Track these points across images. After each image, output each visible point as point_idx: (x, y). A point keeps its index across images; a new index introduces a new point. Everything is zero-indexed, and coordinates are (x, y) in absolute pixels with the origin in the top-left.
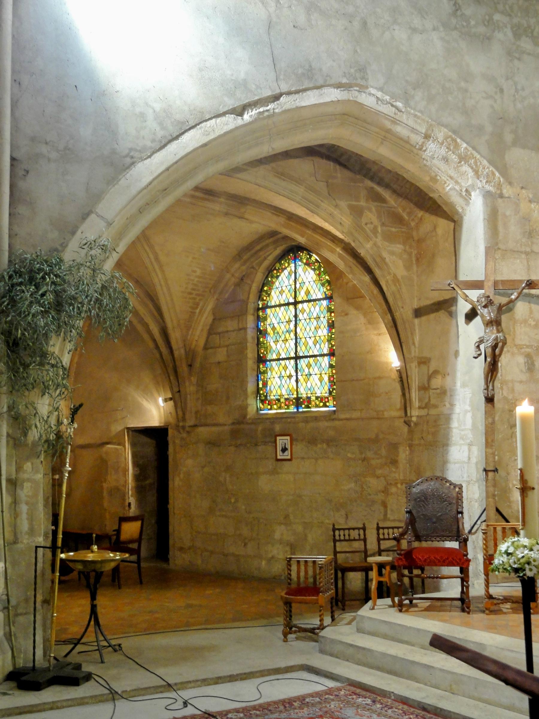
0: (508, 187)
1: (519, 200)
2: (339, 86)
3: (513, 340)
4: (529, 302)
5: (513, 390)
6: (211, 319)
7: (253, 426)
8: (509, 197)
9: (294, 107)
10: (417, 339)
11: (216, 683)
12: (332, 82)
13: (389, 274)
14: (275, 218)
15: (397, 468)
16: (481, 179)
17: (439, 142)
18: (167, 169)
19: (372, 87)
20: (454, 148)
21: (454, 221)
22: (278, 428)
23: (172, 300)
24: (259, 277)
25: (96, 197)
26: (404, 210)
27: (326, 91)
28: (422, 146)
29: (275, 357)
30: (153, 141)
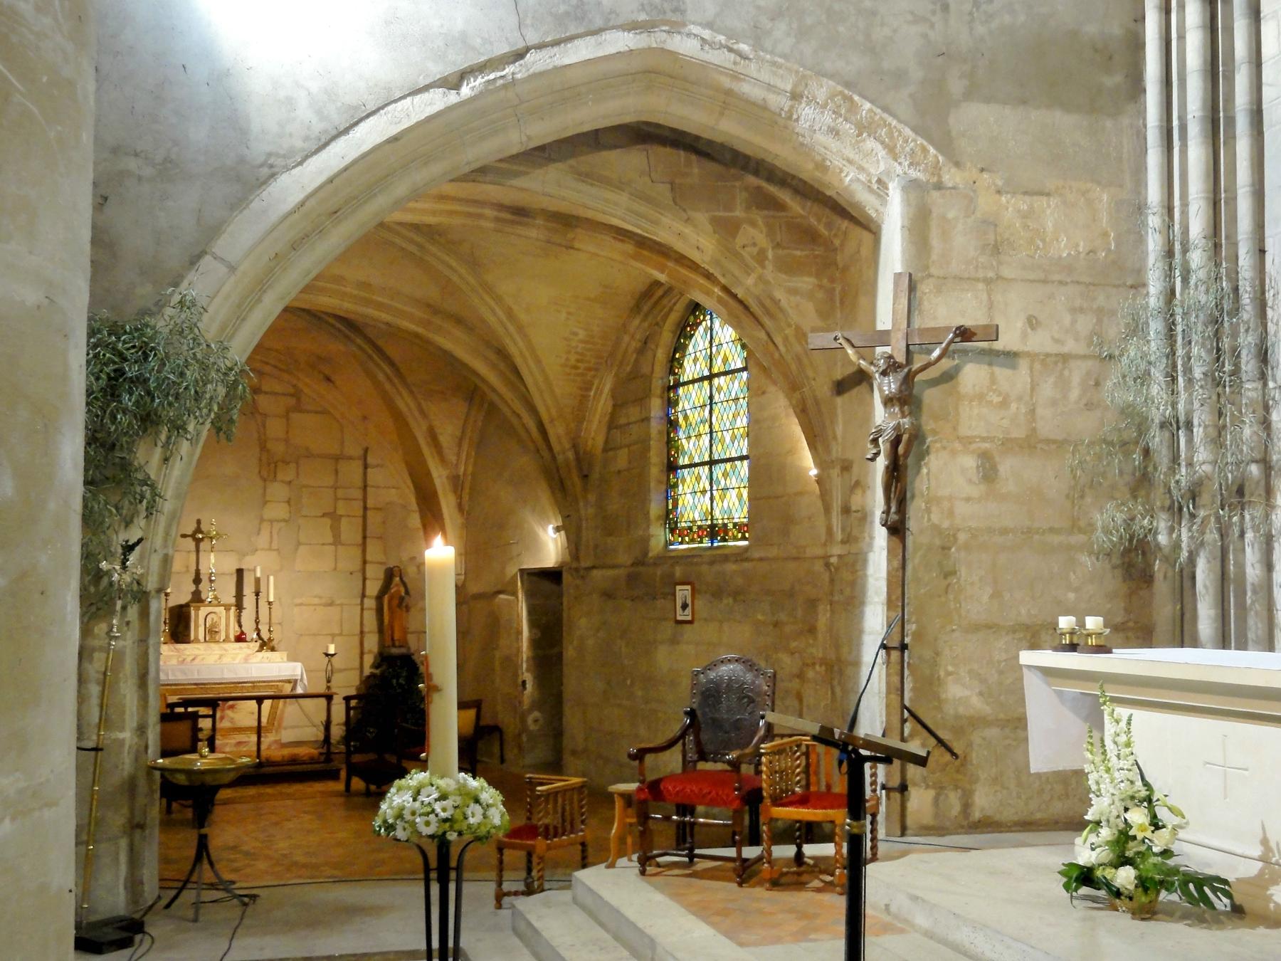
0: (953, 170)
1: (975, 191)
2: (633, 27)
3: (955, 429)
4: (990, 364)
5: (951, 513)
6: (610, 403)
8: (954, 188)
9: (551, 67)
10: (839, 430)
12: (620, 21)
13: (790, 326)
14: (619, 245)
15: (815, 639)
18: (331, 180)
20: (849, 111)
21: (874, 234)
22: (678, 572)
23: (546, 379)
24: (667, 337)
25: (213, 231)
26: (819, 220)
29: (687, 462)
30: (306, 139)
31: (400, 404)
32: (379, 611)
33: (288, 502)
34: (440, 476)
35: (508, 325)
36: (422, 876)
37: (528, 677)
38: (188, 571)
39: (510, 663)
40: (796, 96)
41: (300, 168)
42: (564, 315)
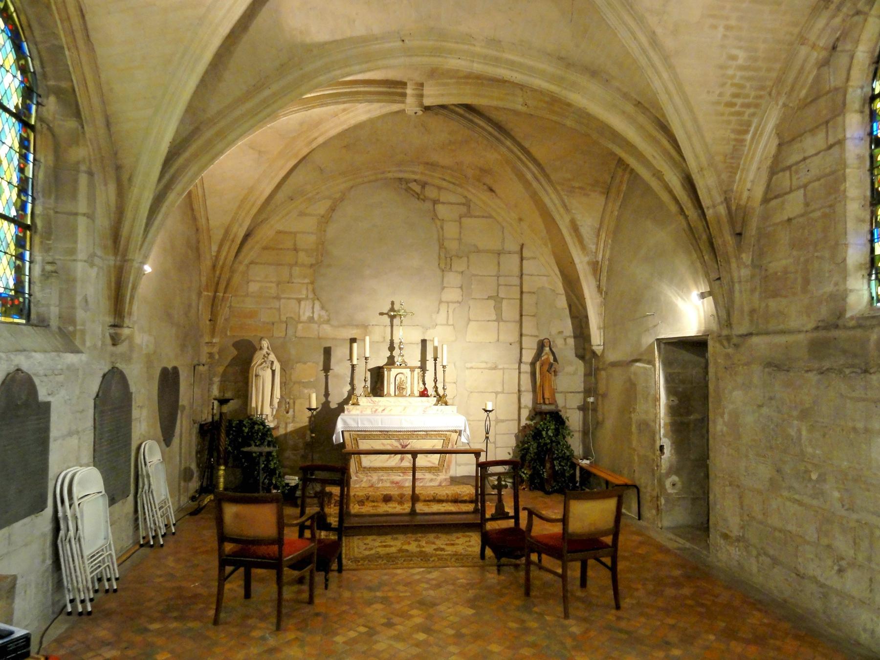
6: (776, 142)
7: (859, 333)
23: (695, 120)
31: (546, 200)
32: (533, 374)
33: (461, 288)
34: (581, 262)
35: (652, 53)
37: (666, 442)
38: (384, 341)
39: (647, 428)
42: (721, 30)
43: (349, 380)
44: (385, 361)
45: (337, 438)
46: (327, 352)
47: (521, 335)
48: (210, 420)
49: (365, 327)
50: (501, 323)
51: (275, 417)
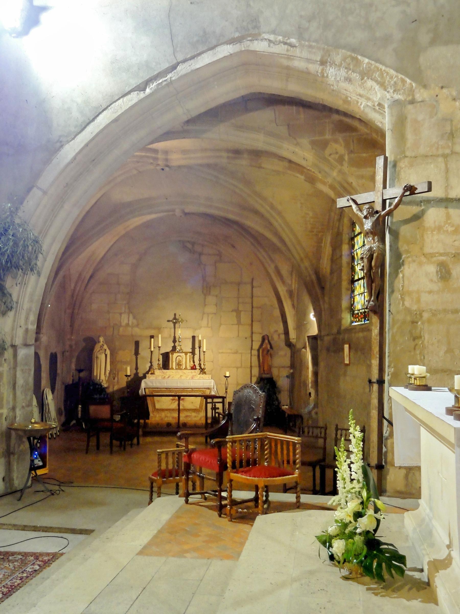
0: (422, 90)
2: (232, 41)
3: (421, 249)
4: (446, 207)
9: (190, 71)
11: (23, 530)
16: (389, 89)
17: (336, 65)
19: (264, 33)
25: (37, 175)
27: (219, 49)
28: (322, 73)
30: (76, 126)
33: (216, 305)
36: (149, 489)
38: (170, 336)
40: (323, 63)
41: (73, 141)
43: (149, 360)
44: (171, 349)
45: (142, 392)
46: (137, 344)
47: (252, 333)
48: (71, 382)
49: (159, 329)
50: (240, 326)
51: (107, 381)
